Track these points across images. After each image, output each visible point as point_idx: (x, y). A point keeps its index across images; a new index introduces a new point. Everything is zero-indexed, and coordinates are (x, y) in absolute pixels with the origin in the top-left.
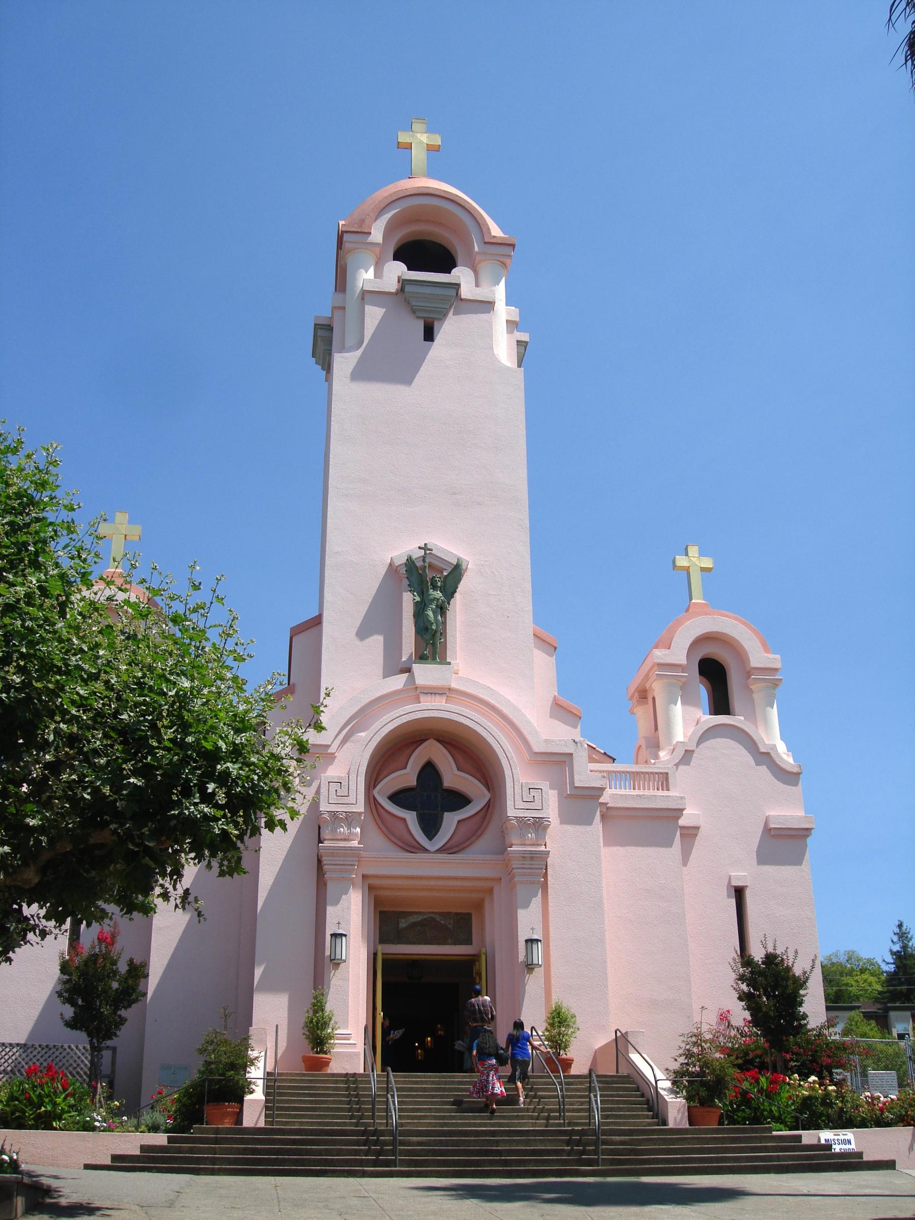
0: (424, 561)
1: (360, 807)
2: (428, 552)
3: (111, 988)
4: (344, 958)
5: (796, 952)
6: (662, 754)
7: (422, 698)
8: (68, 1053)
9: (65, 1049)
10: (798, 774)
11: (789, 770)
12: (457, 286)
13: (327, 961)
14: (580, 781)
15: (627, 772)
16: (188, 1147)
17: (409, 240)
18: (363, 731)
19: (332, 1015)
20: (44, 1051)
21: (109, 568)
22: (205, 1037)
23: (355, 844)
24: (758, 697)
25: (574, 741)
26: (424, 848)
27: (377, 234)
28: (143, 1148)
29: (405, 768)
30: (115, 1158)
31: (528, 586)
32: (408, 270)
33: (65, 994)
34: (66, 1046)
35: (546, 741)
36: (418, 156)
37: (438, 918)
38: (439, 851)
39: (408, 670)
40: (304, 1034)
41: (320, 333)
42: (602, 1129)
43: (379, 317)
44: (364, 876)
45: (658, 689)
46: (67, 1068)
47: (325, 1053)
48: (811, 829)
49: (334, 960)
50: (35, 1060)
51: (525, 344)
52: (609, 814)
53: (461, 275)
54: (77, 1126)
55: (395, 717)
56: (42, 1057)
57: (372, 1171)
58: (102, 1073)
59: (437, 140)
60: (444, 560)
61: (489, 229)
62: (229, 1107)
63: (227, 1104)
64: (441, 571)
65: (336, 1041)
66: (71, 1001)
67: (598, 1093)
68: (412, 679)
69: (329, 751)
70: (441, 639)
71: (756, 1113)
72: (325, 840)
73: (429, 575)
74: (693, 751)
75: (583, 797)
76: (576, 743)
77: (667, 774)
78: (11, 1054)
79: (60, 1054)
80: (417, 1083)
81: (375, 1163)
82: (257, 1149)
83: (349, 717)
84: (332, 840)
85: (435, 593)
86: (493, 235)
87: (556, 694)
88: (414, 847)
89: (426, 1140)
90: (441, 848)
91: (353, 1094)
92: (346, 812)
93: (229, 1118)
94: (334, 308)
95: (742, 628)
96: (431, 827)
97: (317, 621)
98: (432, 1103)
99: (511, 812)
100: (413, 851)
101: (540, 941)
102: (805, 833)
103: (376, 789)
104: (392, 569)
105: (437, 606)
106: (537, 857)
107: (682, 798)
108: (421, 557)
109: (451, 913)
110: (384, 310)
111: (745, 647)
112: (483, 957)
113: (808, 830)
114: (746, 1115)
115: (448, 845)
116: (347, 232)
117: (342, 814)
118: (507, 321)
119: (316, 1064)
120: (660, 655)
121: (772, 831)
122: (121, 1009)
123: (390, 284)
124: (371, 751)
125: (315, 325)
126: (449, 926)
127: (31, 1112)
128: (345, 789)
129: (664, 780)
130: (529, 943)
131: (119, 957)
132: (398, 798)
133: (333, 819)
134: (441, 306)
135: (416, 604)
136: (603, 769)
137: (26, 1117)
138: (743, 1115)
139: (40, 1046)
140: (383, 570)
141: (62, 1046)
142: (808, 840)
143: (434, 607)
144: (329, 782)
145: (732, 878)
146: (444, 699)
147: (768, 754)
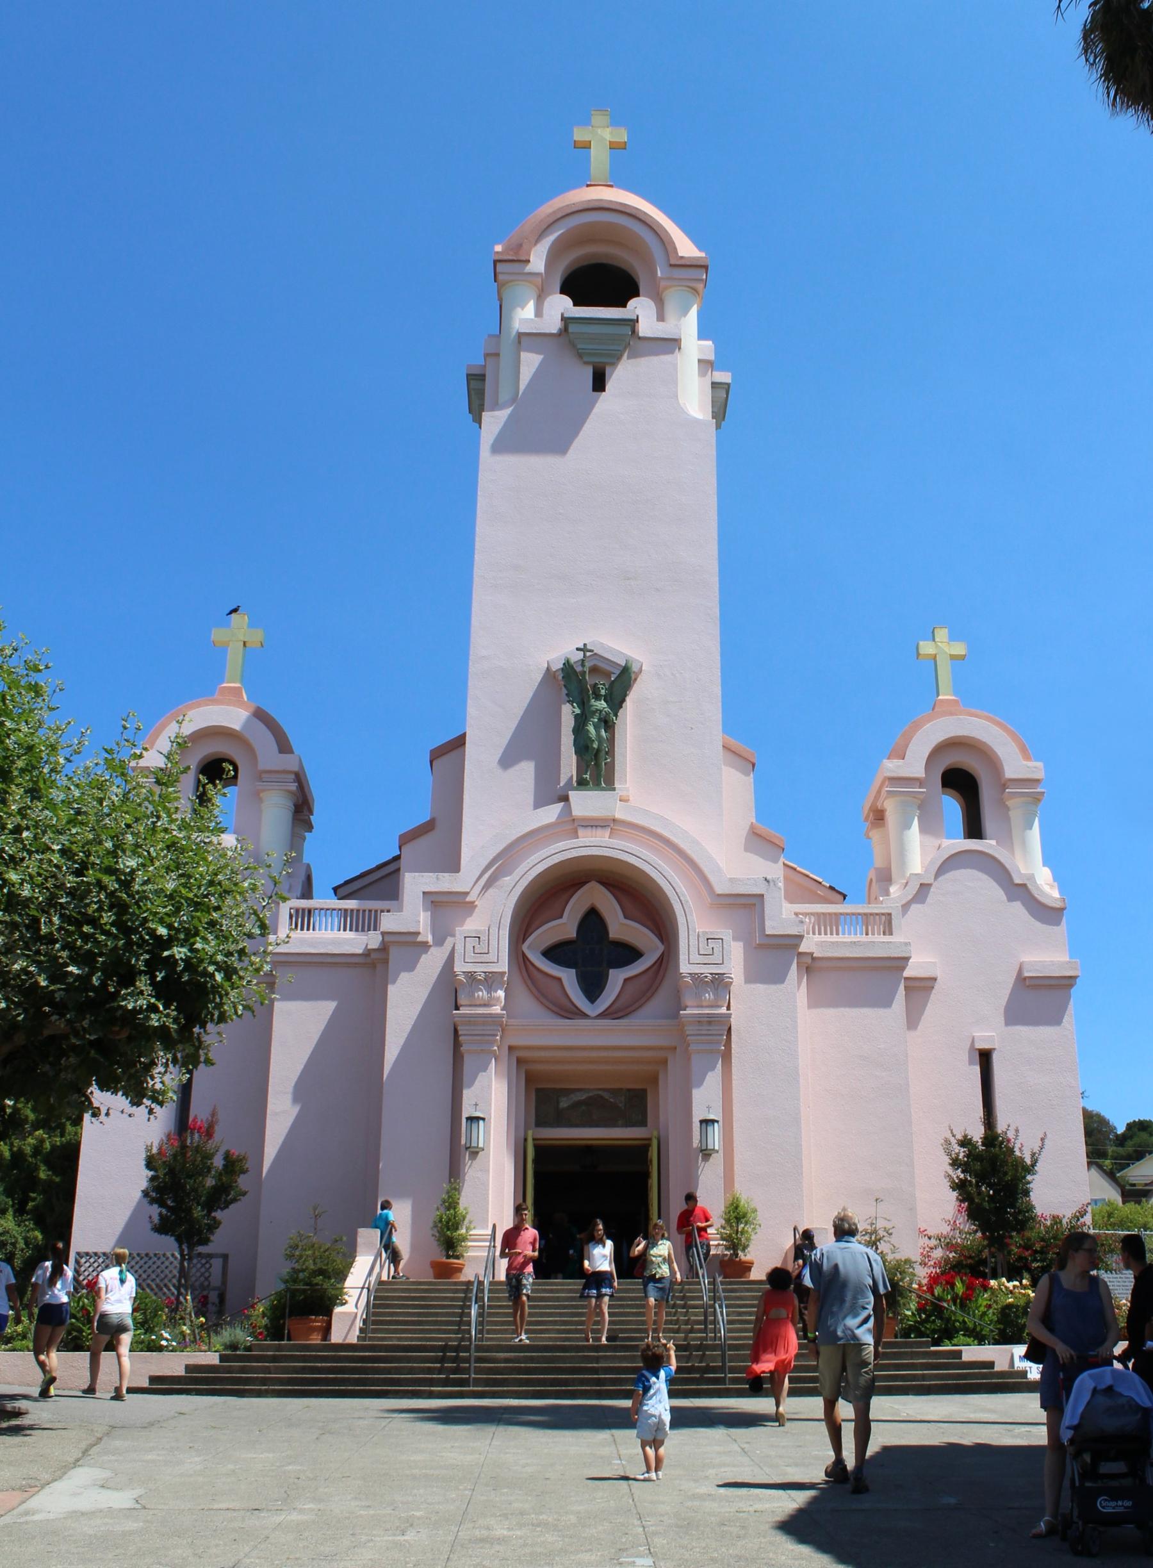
0: (583, 665)
1: (503, 966)
2: (588, 654)
3: (204, 1186)
4: (481, 1145)
5: (1017, 1131)
6: (892, 889)
7: (581, 832)
8: (171, 1263)
9: (168, 1258)
10: (1063, 909)
11: (1050, 905)
12: (633, 323)
13: (463, 1149)
14: (773, 928)
15: (859, 914)
16: (239, 1366)
17: (585, 263)
18: (506, 876)
19: (466, 1213)
20: (142, 1262)
21: (223, 682)
22: (288, 1241)
23: (497, 1010)
24: (1016, 815)
25: (766, 879)
26: (582, 1012)
27: (538, 261)
28: (189, 1368)
29: (561, 917)
30: (153, 1379)
31: (717, 690)
32: (575, 305)
33: (151, 1193)
34: (169, 1254)
35: (731, 880)
36: (599, 157)
37: (606, 1095)
38: (602, 1015)
39: (565, 799)
40: (433, 1235)
41: (473, 384)
42: (728, 1344)
43: (536, 365)
44: (511, 1048)
45: (891, 808)
46: (170, 1281)
47: (458, 1257)
48: (1075, 978)
49: (469, 1148)
50: (199, 1266)
51: (726, 386)
52: (811, 966)
53: (640, 308)
54: (140, 1346)
55: (544, 857)
56: (149, 1267)
57: (440, 1391)
58: (211, 1284)
59: (622, 136)
60: (612, 661)
61: (675, 248)
62: (315, 1321)
63: (314, 1317)
64: (608, 674)
65: (470, 1244)
66: (161, 1202)
67: (724, 1303)
68: (568, 809)
69: (469, 899)
70: (606, 759)
71: (946, 1325)
72: (461, 1006)
73: (590, 680)
74: (930, 885)
75: (778, 947)
76: (768, 882)
77: (890, 914)
78: (96, 1265)
79: (145, 1263)
80: (551, 1291)
81: (446, 1382)
82: (317, 1367)
83: (491, 858)
84: (470, 1006)
85: (597, 703)
86: (680, 255)
87: (754, 821)
88: (566, 1011)
89: (515, 1356)
90: (604, 1011)
91: (679, 1305)
92: (485, 973)
93: (316, 1333)
94: (487, 355)
95: (996, 730)
96: (592, 987)
97: (459, 742)
98: (561, 1315)
99: (685, 968)
100: (569, 1016)
101: (717, 1122)
102: (1067, 983)
103: (525, 944)
104: (549, 673)
105: (600, 719)
106: (715, 1021)
107: (907, 944)
108: (579, 661)
109: (622, 1089)
110: (542, 357)
111: (999, 754)
112: (655, 1143)
113: (1073, 978)
114: (936, 1328)
115: (610, 1010)
116: (501, 261)
117: (480, 975)
118: (699, 361)
119: (445, 1271)
120: (892, 767)
121: (1027, 980)
122: (216, 1211)
123: (553, 325)
124: (516, 898)
125: (468, 375)
126: (620, 1105)
127: (89, 1331)
128: (484, 945)
129: (887, 923)
130: (704, 1125)
131: (217, 1151)
132: (555, 953)
133: (470, 981)
134: (612, 347)
135: (576, 717)
136: (810, 911)
137: (84, 1336)
138: (933, 1327)
139: (138, 1255)
140: (538, 677)
141: (164, 1255)
142: (1073, 991)
143: (596, 720)
144: (465, 937)
145: (976, 1039)
146: (607, 832)
147: (1024, 885)
